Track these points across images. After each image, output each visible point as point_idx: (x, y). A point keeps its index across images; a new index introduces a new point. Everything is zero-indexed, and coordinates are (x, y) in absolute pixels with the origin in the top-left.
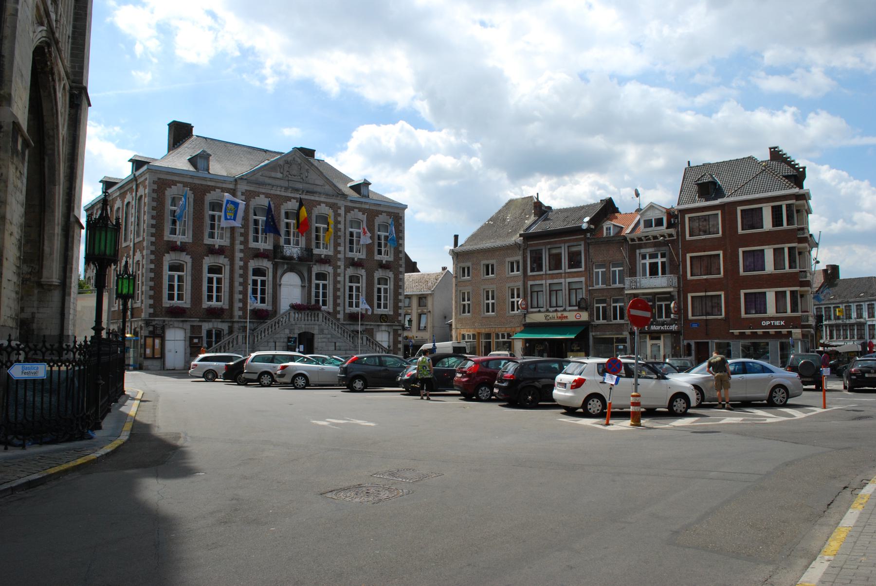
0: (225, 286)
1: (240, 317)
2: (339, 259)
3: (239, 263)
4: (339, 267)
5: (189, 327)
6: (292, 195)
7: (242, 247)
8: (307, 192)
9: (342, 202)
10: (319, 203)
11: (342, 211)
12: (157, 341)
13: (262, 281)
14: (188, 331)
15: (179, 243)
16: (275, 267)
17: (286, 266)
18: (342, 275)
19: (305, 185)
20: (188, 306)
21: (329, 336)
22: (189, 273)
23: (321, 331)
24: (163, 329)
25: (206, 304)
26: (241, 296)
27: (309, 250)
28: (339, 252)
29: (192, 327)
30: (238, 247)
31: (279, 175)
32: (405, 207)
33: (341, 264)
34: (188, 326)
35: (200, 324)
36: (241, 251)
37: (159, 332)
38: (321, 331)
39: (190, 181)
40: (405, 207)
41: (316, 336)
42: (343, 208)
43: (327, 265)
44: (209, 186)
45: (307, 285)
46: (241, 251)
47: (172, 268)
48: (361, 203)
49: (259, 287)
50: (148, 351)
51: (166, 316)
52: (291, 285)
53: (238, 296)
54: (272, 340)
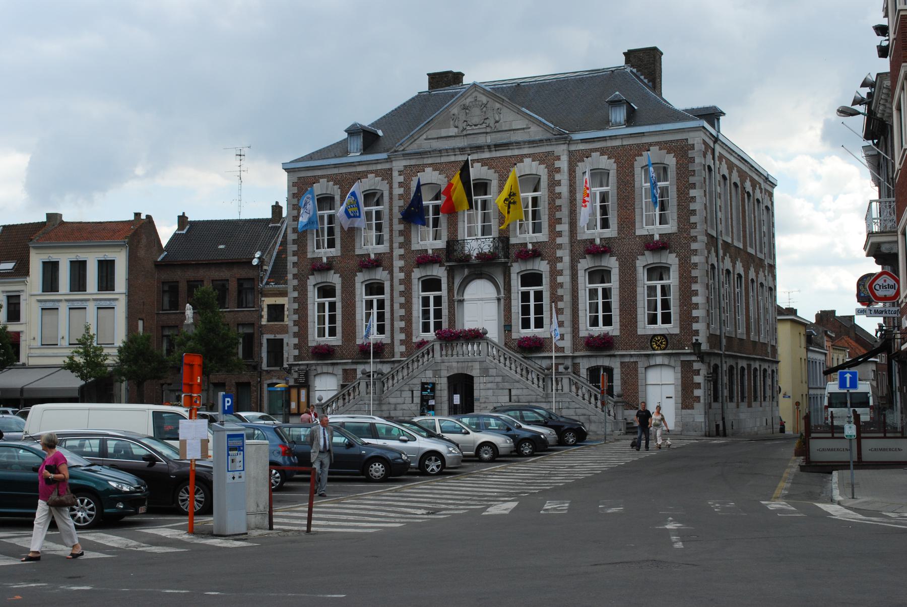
0: (543, 208)
1: (402, 354)
2: (560, 246)
7: (402, 251)
8: (496, 146)
9: (565, 147)
10: (520, 158)
12: (303, 392)
14: (340, 377)
15: (657, 237)
16: (451, 273)
17: (466, 272)
19: (494, 136)
20: (617, 333)
22: (639, 284)
23: (485, 372)
24: (307, 375)
27: (503, 239)
29: (345, 371)
30: (398, 252)
31: (453, 131)
33: (564, 254)
34: (339, 370)
35: (353, 367)
36: (401, 257)
37: (302, 380)
38: (485, 372)
39: (336, 171)
41: (476, 380)
42: (565, 158)
43: (538, 260)
44: (359, 173)
45: (502, 295)
46: (401, 257)
48: (604, 139)
49: (532, 303)
50: (293, 405)
51: (313, 359)
52: (482, 300)
54: (407, 388)
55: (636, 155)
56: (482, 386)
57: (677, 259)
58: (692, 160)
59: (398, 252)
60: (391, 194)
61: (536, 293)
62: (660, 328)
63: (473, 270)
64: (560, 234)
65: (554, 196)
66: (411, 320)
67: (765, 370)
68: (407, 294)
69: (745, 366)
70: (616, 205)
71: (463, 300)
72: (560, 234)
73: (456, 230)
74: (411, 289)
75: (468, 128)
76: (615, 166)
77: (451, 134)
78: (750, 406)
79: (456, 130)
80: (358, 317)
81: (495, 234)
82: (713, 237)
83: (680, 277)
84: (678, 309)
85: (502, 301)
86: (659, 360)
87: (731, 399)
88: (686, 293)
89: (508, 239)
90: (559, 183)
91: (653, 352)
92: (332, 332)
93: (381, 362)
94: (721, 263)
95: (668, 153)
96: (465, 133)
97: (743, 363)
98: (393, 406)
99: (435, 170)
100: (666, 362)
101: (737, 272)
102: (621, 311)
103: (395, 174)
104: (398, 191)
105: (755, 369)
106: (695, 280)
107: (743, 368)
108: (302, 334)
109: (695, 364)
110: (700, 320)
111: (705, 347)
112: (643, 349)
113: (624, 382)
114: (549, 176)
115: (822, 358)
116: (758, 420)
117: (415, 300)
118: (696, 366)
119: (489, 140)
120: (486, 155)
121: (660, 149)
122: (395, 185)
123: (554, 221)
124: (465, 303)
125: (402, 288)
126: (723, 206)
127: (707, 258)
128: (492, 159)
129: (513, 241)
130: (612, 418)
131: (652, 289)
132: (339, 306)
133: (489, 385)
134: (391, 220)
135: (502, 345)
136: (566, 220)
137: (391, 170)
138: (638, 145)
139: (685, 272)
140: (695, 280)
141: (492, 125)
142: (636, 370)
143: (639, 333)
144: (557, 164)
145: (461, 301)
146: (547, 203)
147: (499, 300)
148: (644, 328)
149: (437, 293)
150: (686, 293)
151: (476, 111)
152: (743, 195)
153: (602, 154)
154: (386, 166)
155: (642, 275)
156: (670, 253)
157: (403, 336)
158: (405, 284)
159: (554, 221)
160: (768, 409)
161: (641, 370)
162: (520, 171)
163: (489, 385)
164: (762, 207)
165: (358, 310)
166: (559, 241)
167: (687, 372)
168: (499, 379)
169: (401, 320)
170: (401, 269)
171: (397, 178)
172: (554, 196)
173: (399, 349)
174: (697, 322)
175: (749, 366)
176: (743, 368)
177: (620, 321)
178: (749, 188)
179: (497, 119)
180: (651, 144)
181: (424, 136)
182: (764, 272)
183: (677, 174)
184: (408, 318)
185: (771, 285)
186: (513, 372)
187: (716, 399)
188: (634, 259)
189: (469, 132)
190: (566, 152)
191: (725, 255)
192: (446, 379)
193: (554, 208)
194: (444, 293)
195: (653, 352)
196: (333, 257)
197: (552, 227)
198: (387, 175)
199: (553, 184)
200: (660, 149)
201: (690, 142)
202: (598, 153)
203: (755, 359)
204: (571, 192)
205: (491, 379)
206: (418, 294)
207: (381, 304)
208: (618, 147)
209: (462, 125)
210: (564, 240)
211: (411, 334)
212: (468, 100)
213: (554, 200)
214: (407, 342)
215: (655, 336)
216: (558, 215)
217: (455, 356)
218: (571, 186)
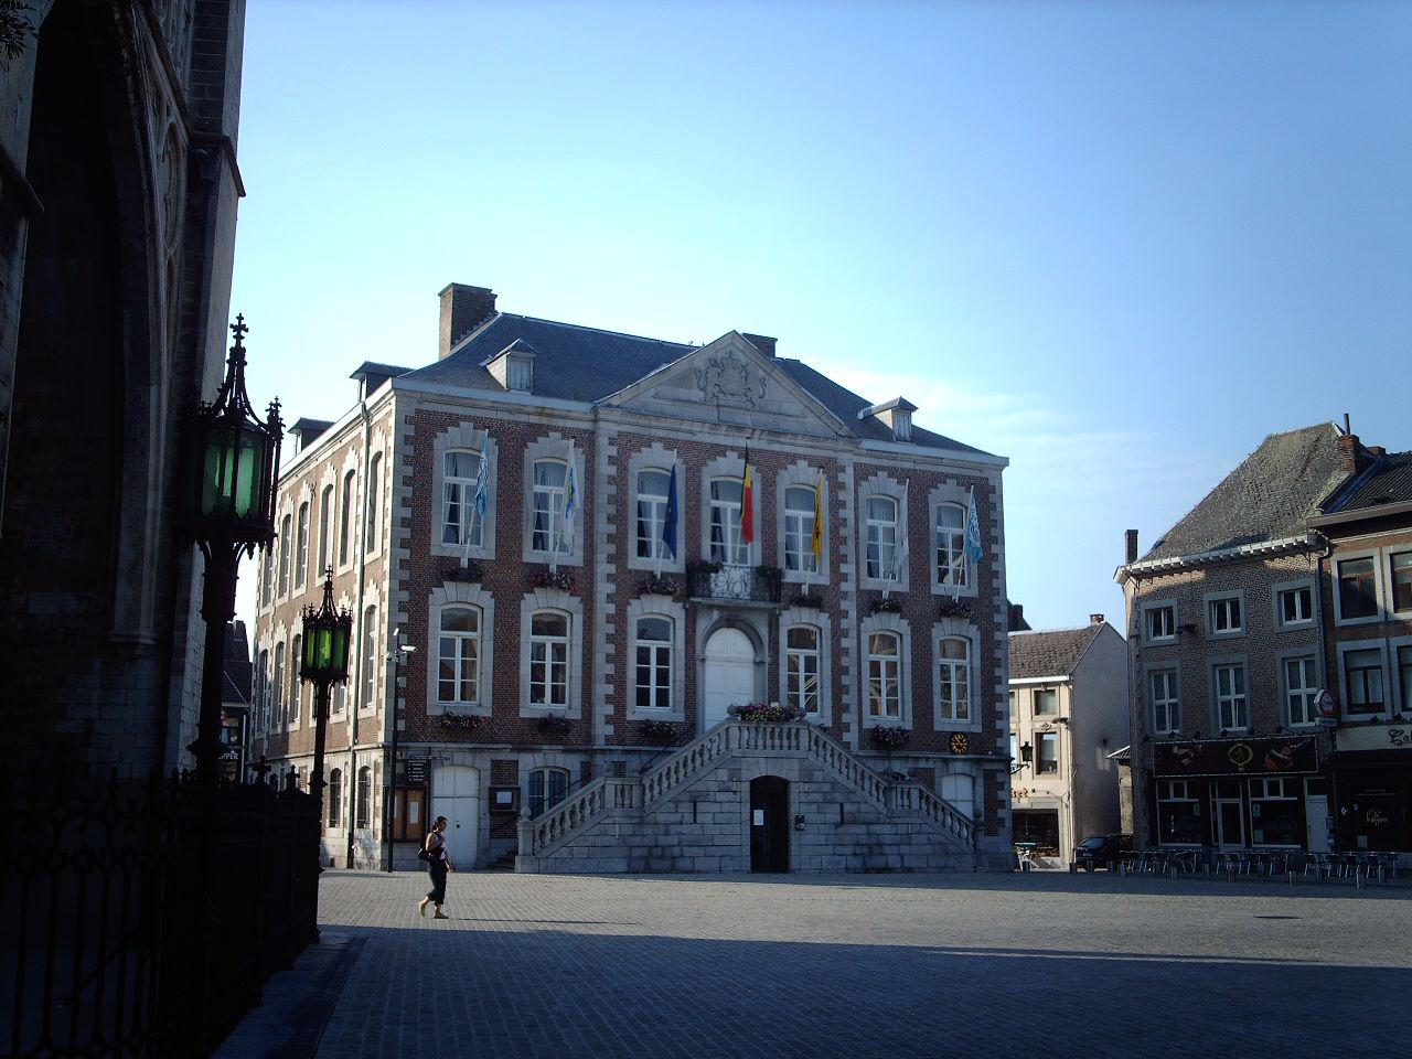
1: (607, 738)
2: (845, 595)
3: (605, 608)
4: (845, 614)
5: (488, 765)
6: (728, 441)
7: (612, 569)
11: (848, 478)
13: (659, 651)
14: (487, 774)
18: (853, 634)
21: (827, 787)
22: (489, 634)
25: (529, 710)
26: (610, 689)
28: (844, 577)
29: (496, 764)
30: (604, 568)
31: (698, 395)
32: (1004, 462)
33: (849, 606)
34: (485, 761)
36: (610, 578)
38: (807, 776)
39: (491, 414)
40: (1004, 462)
42: (850, 470)
46: (610, 578)
47: (540, 627)
53: (603, 689)
56: (803, 798)
61: (554, 646)
63: (725, 613)
64: (844, 577)
75: (721, 395)
77: (693, 399)
91: (954, 756)
93: (564, 751)
98: (662, 829)
103: (603, 441)
109: (999, 775)
114: (831, 492)
131: (539, 651)
138: (932, 473)
143: (935, 729)
145: (703, 661)
147: (758, 664)
149: (662, 644)
153: (890, 476)
154: (587, 426)
156: (901, 618)
158: (615, 623)
163: (814, 797)
168: (827, 787)
169: (608, 682)
180: (947, 476)
181: (653, 392)
188: (930, 626)
189: (721, 402)
192: (746, 787)
196: (481, 561)
205: (814, 787)
214: (617, 719)
215: (956, 733)
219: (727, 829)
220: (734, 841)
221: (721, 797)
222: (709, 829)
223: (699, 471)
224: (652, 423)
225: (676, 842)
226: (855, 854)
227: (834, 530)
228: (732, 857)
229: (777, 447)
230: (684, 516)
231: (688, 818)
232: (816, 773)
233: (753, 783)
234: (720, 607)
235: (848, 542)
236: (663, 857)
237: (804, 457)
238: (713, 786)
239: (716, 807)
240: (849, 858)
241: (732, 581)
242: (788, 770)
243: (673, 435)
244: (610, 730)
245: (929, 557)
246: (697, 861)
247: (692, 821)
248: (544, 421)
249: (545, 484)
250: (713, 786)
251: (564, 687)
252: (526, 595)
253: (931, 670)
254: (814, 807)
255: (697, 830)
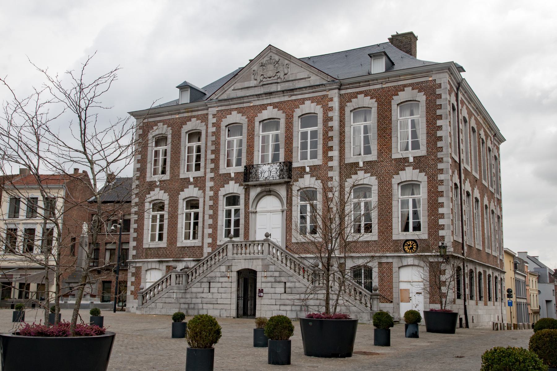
2: (331, 168)
6: (269, 101)
7: (212, 175)
10: (302, 101)
11: (335, 104)
21: (277, 274)
22: (394, 198)
31: (253, 83)
33: (335, 174)
34: (163, 267)
36: (212, 179)
38: (266, 268)
41: (259, 275)
42: (336, 100)
55: (393, 95)
56: (264, 280)
57: (426, 177)
58: (440, 96)
59: (210, 175)
60: (207, 132)
61: (195, 213)
62: (411, 235)
64: (331, 159)
65: (327, 129)
66: (217, 227)
67: (496, 278)
68: (214, 207)
69: (482, 272)
70: (376, 135)
71: (256, 212)
72: (331, 159)
73: (253, 158)
74: (217, 203)
75: (264, 80)
76: (376, 104)
77: (251, 85)
78: (486, 304)
79: (255, 82)
80: (179, 226)
81: (282, 159)
82: (456, 162)
83: (428, 192)
84: (426, 219)
85: (285, 212)
86: (410, 261)
87: (472, 298)
88: (434, 205)
89: (291, 163)
90: (331, 119)
91: (405, 255)
92: (161, 238)
94: (463, 185)
95: (419, 91)
96: (262, 83)
97: (480, 269)
99: (239, 113)
100: (416, 262)
101: (474, 196)
102: (379, 220)
103: (210, 117)
104: (212, 129)
105: (489, 276)
106: (441, 194)
107: (480, 274)
108: (139, 239)
110: (446, 227)
111: (450, 250)
112: (396, 251)
113: (381, 279)
114: (324, 113)
115: (523, 279)
116: (492, 316)
117: (220, 213)
118: (443, 267)
119: (279, 88)
120: (276, 100)
121: (413, 89)
122: (210, 125)
123: (327, 149)
124: (257, 214)
125: (211, 203)
126: (464, 140)
127: (452, 176)
128: (281, 102)
129: (295, 165)
130: (369, 308)
132: (166, 216)
133: (270, 279)
134: (206, 152)
135: (284, 248)
136: (336, 147)
137: (207, 114)
138: (395, 87)
139: (433, 187)
140: (441, 194)
141: (282, 77)
142: (391, 270)
144: (330, 104)
146: (321, 135)
147: (283, 211)
148: (398, 234)
150: (434, 205)
151: (271, 67)
152: (479, 142)
153: (366, 96)
154: (205, 112)
155: (397, 191)
157: (210, 240)
158: (214, 200)
159: (327, 149)
160: (499, 308)
161: (395, 269)
162: (302, 111)
163: (270, 279)
164: (492, 155)
165: (180, 221)
166: (330, 164)
167: (435, 272)
169: (210, 228)
170: (211, 189)
171: (212, 120)
172: (327, 129)
173: (207, 250)
174: (443, 229)
175: (485, 272)
176: (480, 274)
177: (379, 228)
178: (483, 136)
179: (286, 72)
180: (405, 86)
181: (232, 88)
182: (494, 202)
183: (427, 108)
184: (214, 227)
185: (499, 214)
186: (288, 268)
187: (459, 297)
189: (264, 83)
190: (337, 95)
191: (465, 179)
192: (234, 275)
193: (327, 138)
194: (241, 206)
195: (405, 255)
197: (325, 153)
198: (204, 119)
199: (327, 119)
200: (413, 89)
201: (438, 82)
202: (363, 95)
203: (488, 267)
204: (340, 126)
205: (269, 274)
206: (223, 207)
207: (196, 216)
208: (379, 89)
209: (259, 78)
210: (335, 163)
211: (216, 239)
212: (265, 59)
213: (327, 133)
214: (213, 245)
215: (407, 240)
216: (330, 144)
217: (243, 255)
218: (341, 121)
219: (224, 295)
220: (228, 301)
221: (222, 280)
222: (216, 296)
223: (254, 120)
224: (231, 103)
225: (200, 302)
226: (292, 310)
227: (325, 133)
228: (226, 310)
229: (294, 98)
230: (246, 144)
231: (206, 290)
232: (271, 266)
233: (239, 273)
234: (261, 185)
235: (334, 139)
236: (194, 309)
237: (309, 99)
238: (218, 274)
239: (219, 285)
240: (288, 312)
241: (268, 171)
242: (256, 266)
243: (241, 106)
244: (210, 250)
245: (391, 138)
246: (209, 310)
247: (208, 291)
248: (189, 114)
249: (413, 115)
250: (218, 274)
251: (186, 229)
252: (181, 193)
253: (391, 204)
254: (269, 284)
255: (210, 295)
